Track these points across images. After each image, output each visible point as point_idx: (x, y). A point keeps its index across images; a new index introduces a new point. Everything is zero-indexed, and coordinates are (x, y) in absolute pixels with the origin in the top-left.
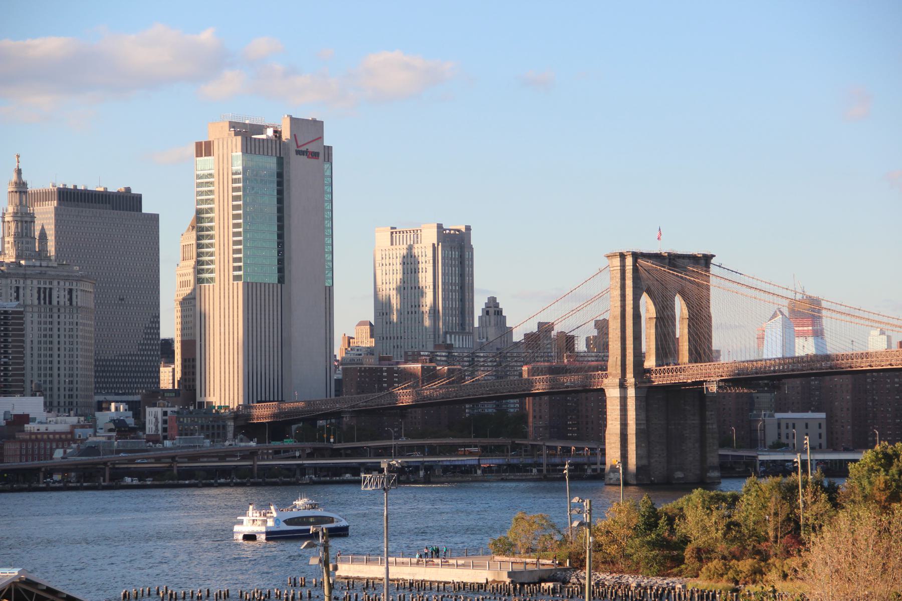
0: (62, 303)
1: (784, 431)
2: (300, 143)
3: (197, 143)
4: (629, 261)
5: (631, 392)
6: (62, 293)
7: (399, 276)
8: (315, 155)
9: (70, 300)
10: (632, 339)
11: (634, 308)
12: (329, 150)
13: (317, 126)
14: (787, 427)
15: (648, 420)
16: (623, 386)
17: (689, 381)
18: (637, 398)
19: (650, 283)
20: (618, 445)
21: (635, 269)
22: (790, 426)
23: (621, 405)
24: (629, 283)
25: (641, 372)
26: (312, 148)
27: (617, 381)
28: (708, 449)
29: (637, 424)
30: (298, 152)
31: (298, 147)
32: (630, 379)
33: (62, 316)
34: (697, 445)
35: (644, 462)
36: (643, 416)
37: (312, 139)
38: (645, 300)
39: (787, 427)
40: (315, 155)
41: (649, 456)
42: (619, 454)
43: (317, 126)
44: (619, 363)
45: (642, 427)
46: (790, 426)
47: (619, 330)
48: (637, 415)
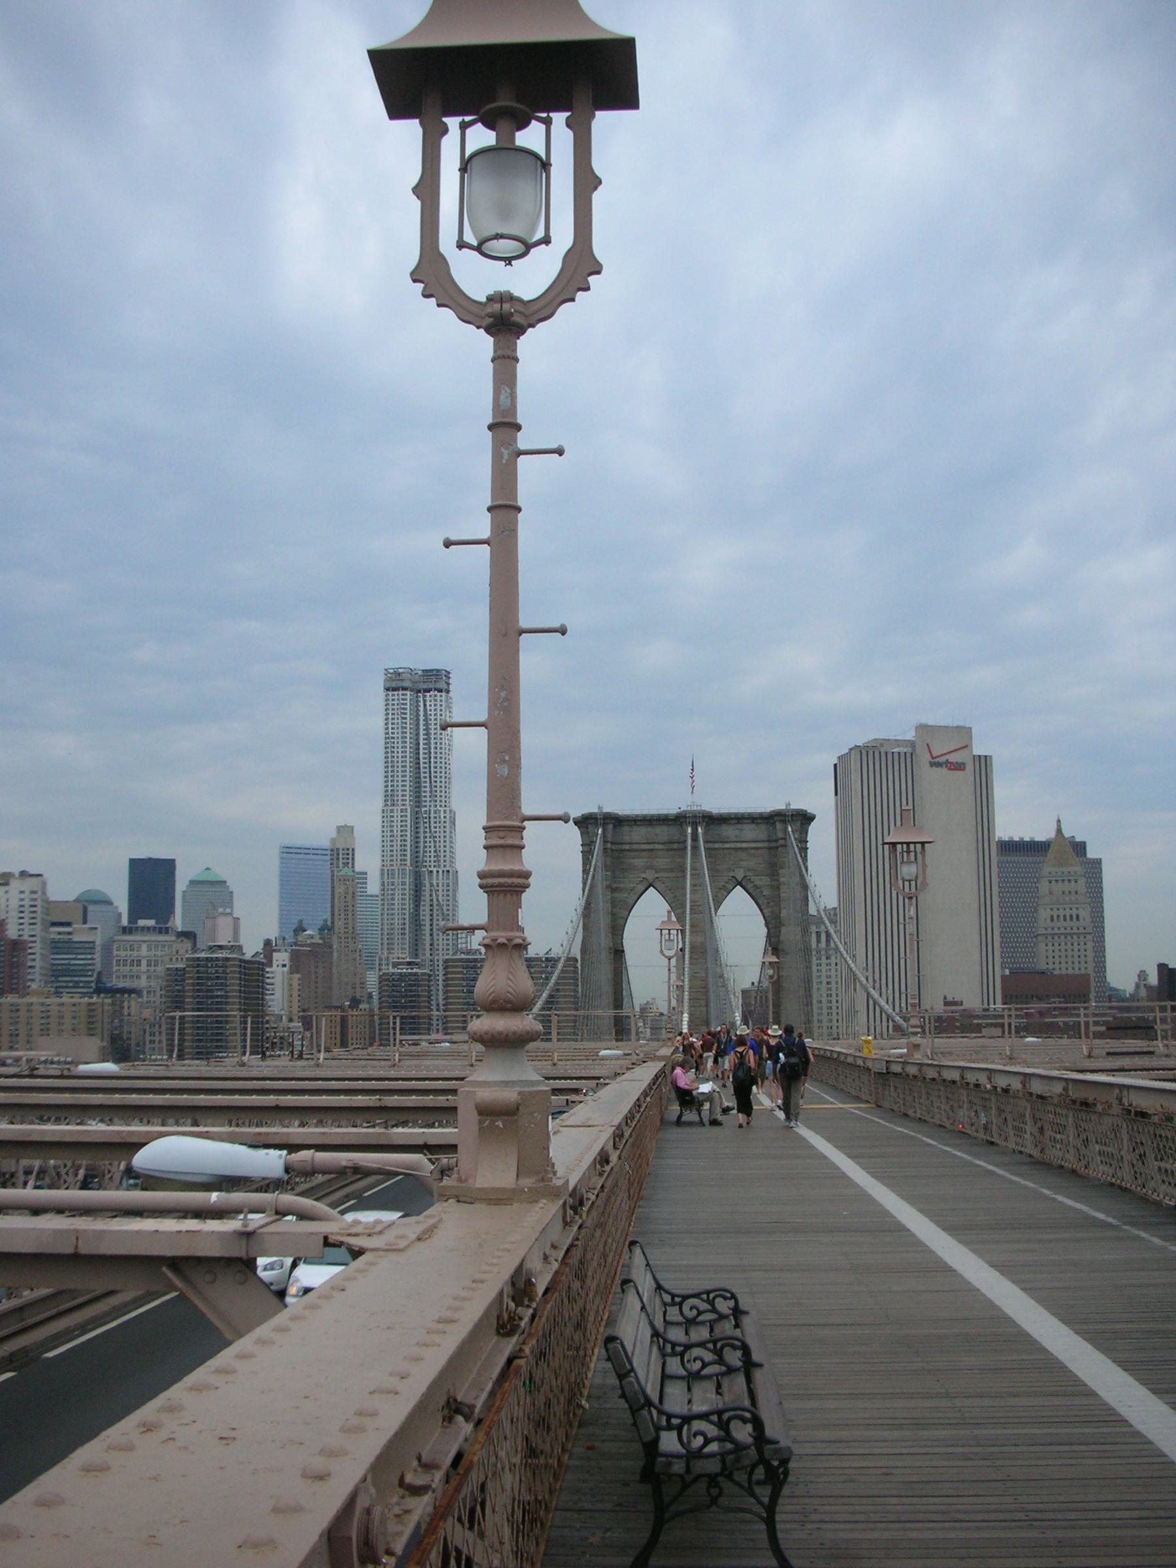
8: (960, 767)
12: (984, 764)
13: (964, 732)
26: (954, 758)
40: (960, 767)
43: (964, 732)
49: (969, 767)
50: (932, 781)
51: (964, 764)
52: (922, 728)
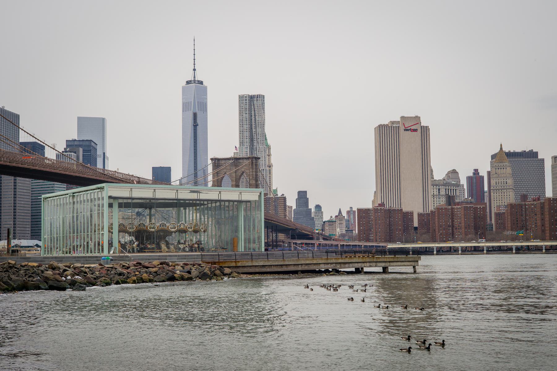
0: (435, 194)
3: (300, 193)
6: (435, 190)
8: (415, 130)
9: (439, 192)
13: (417, 118)
26: (413, 128)
33: (435, 199)
40: (415, 130)
43: (417, 118)
49: (419, 130)
50: (405, 136)
52: (402, 118)
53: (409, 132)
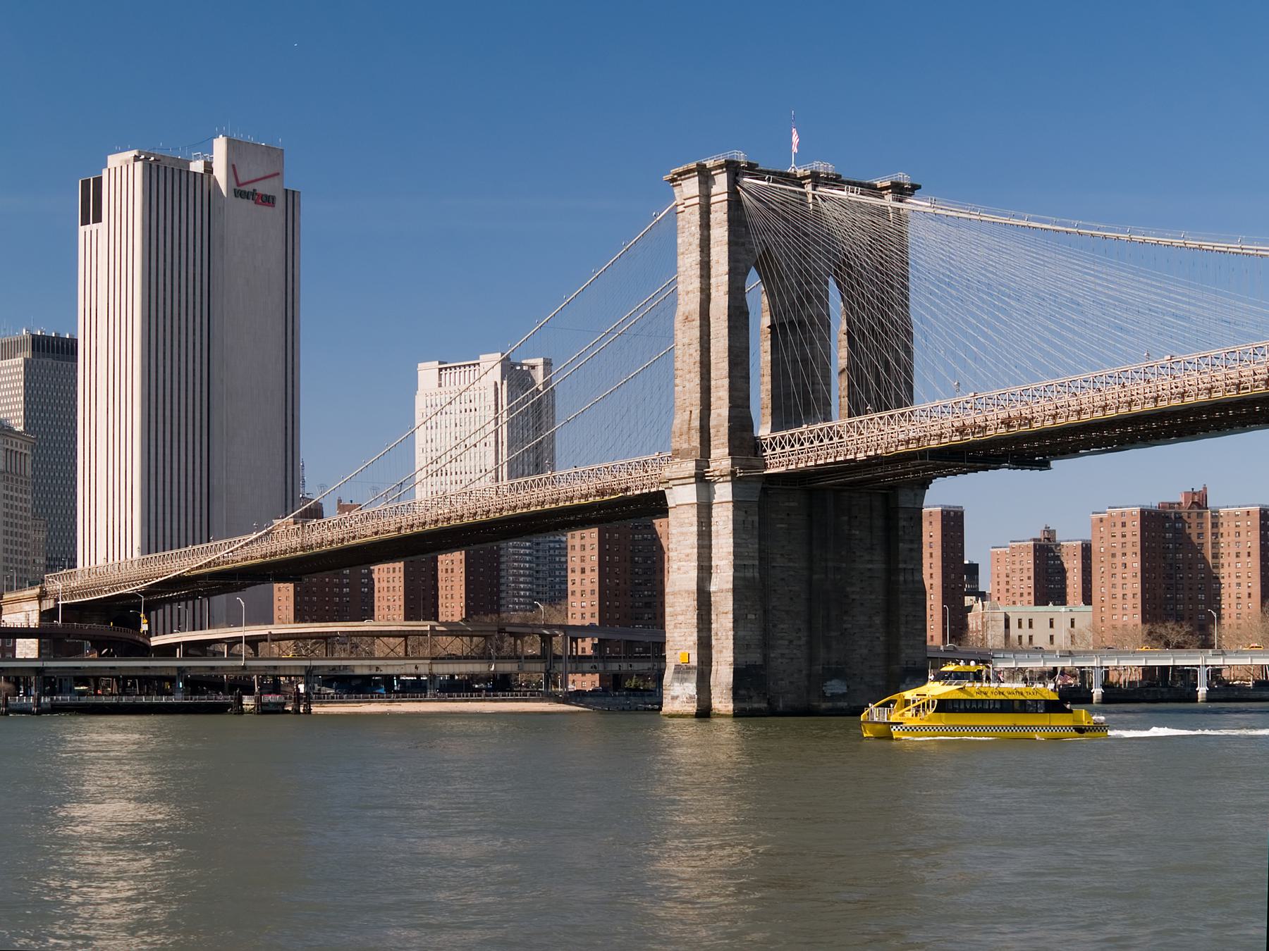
1: (1014, 631)
2: (241, 180)
4: (721, 183)
5: (723, 492)
7: (696, 634)
8: (268, 200)
10: (725, 365)
11: (730, 293)
12: (292, 197)
14: (1020, 626)
15: (764, 558)
16: (702, 480)
17: (861, 456)
18: (738, 504)
19: (770, 238)
20: (692, 618)
21: (735, 203)
22: (1025, 624)
23: (700, 524)
24: (720, 234)
25: (744, 443)
26: (262, 188)
27: (690, 467)
28: (903, 629)
29: (736, 568)
30: (239, 193)
31: (238, 185)
32: (721, 459)
34: (878, 620)
35: (755, 657)
36: (753, 546)
37: (262, 175)
38: (754, 282)
39: (1020, 626)
40: (268, 200)
41: (766, 643)
42: (695, 637)
44: (696, 423)
45: (749, 574)
46: (1025, 624)
47: (696, 345)
48: (736, 545)
49: (280, 202)
51: (274, 198)
53: (248, 204)
